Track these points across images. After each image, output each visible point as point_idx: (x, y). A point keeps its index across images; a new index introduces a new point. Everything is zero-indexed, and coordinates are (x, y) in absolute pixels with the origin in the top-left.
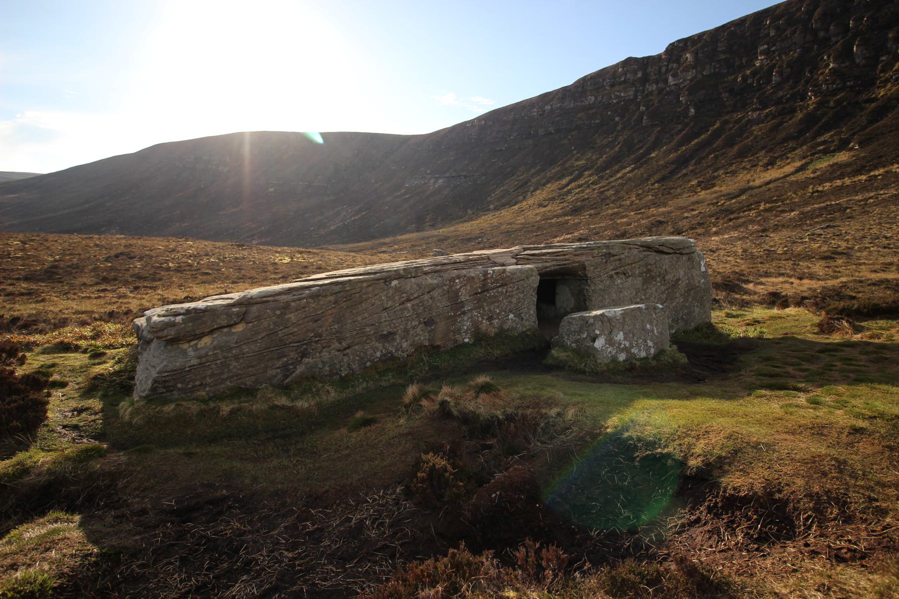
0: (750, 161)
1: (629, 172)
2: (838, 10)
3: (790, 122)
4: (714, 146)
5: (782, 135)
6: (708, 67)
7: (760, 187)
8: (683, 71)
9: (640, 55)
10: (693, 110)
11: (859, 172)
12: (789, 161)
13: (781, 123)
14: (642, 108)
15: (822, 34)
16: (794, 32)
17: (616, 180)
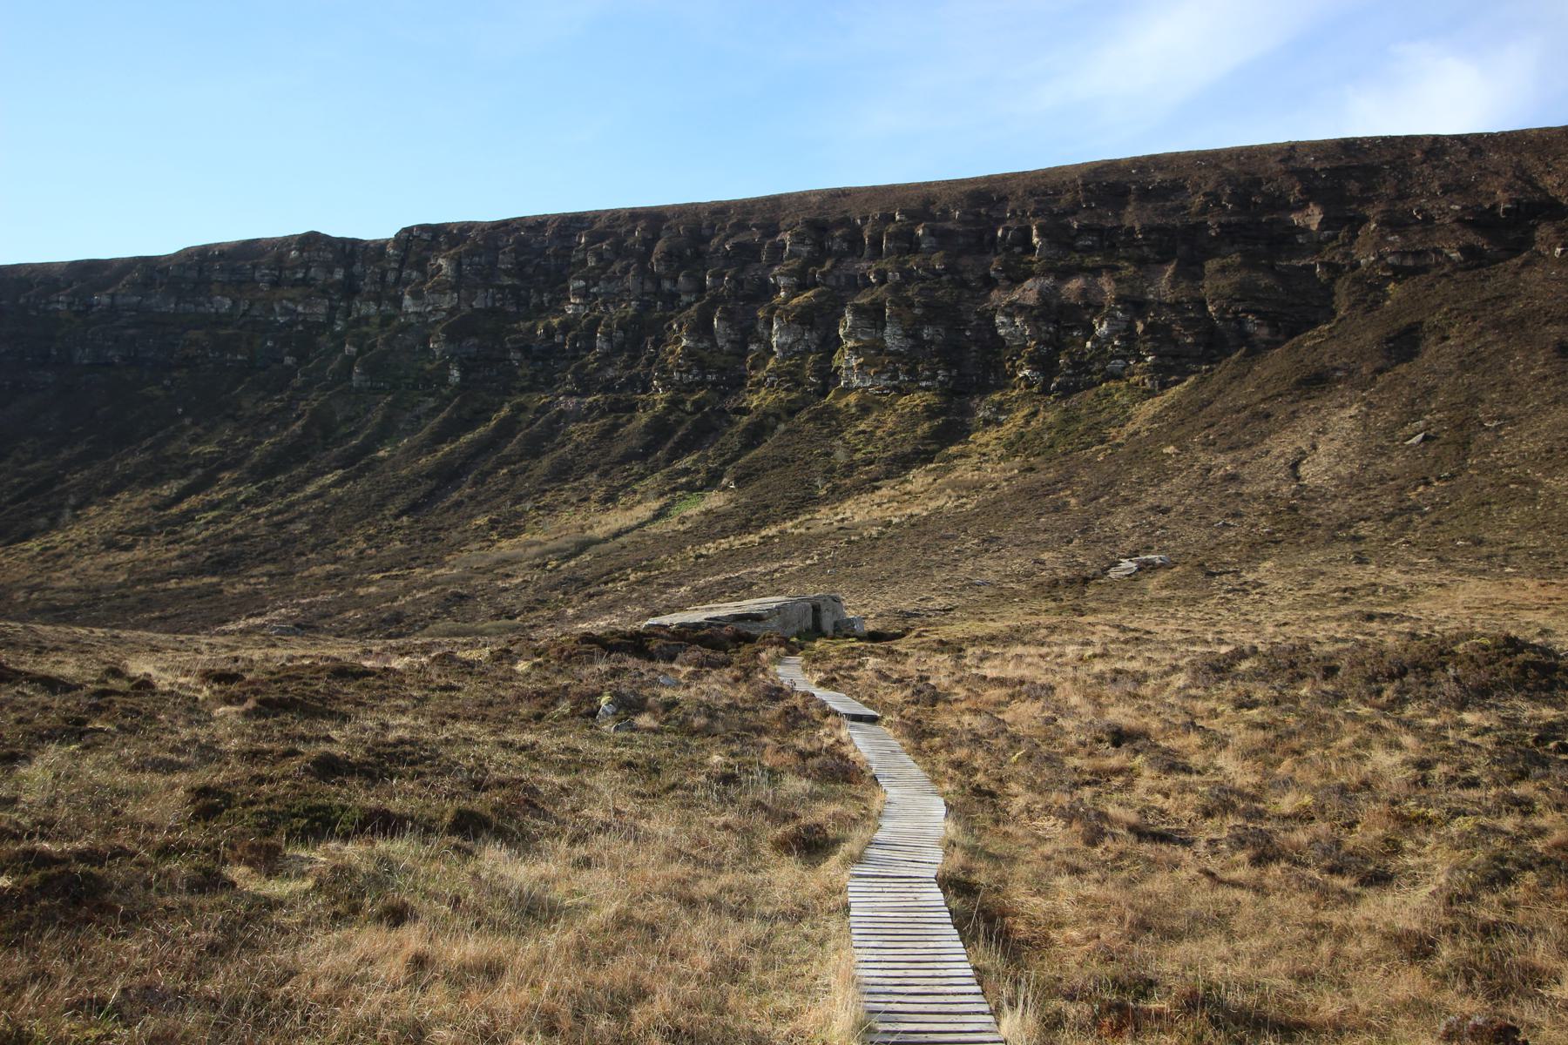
0: (574, 489)
1: (335, 484)
2: (688, 252)
3: (630, 427)
4: (506, 451)
5: (619, 449)
6: (481, 293)
7: (606, 540)
8: (433, 290)
9: (335, 232)
10: (456, 373)
11: (744, 528)
12: (638, 497)
13: (615, 427)
14: (349, 349)
15: (667, 285)
16: (625, 271)
17: (307, 499)
